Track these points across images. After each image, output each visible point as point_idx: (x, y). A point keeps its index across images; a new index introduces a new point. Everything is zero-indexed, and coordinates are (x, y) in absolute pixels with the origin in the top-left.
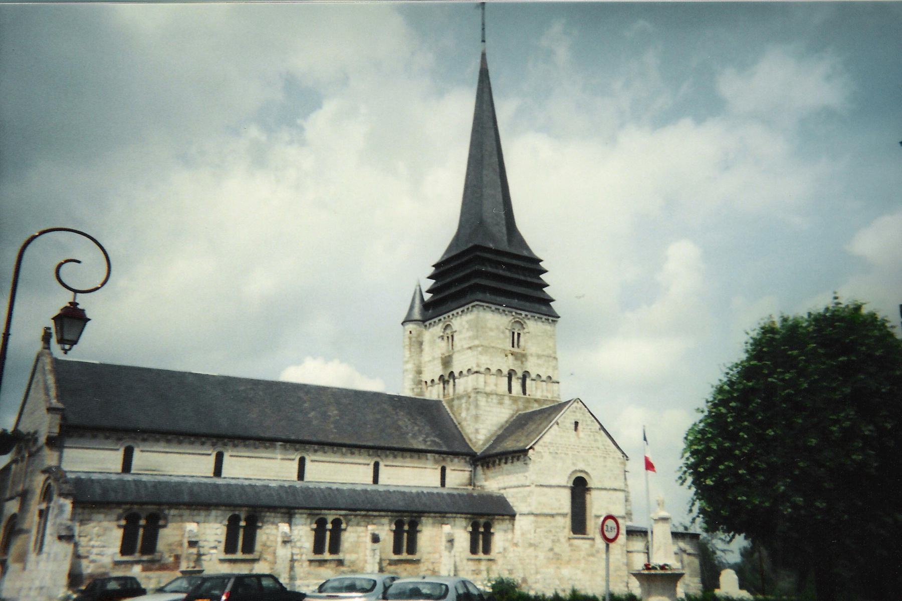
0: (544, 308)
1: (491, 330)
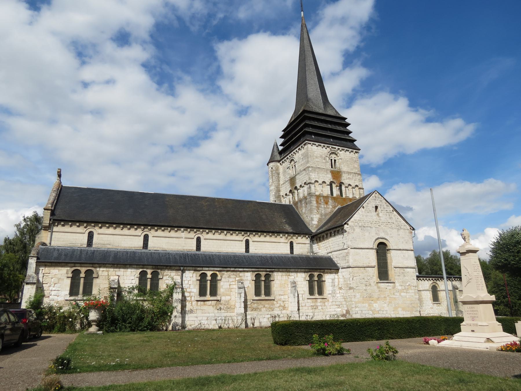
0: (349, 144)
1: (317, 157)
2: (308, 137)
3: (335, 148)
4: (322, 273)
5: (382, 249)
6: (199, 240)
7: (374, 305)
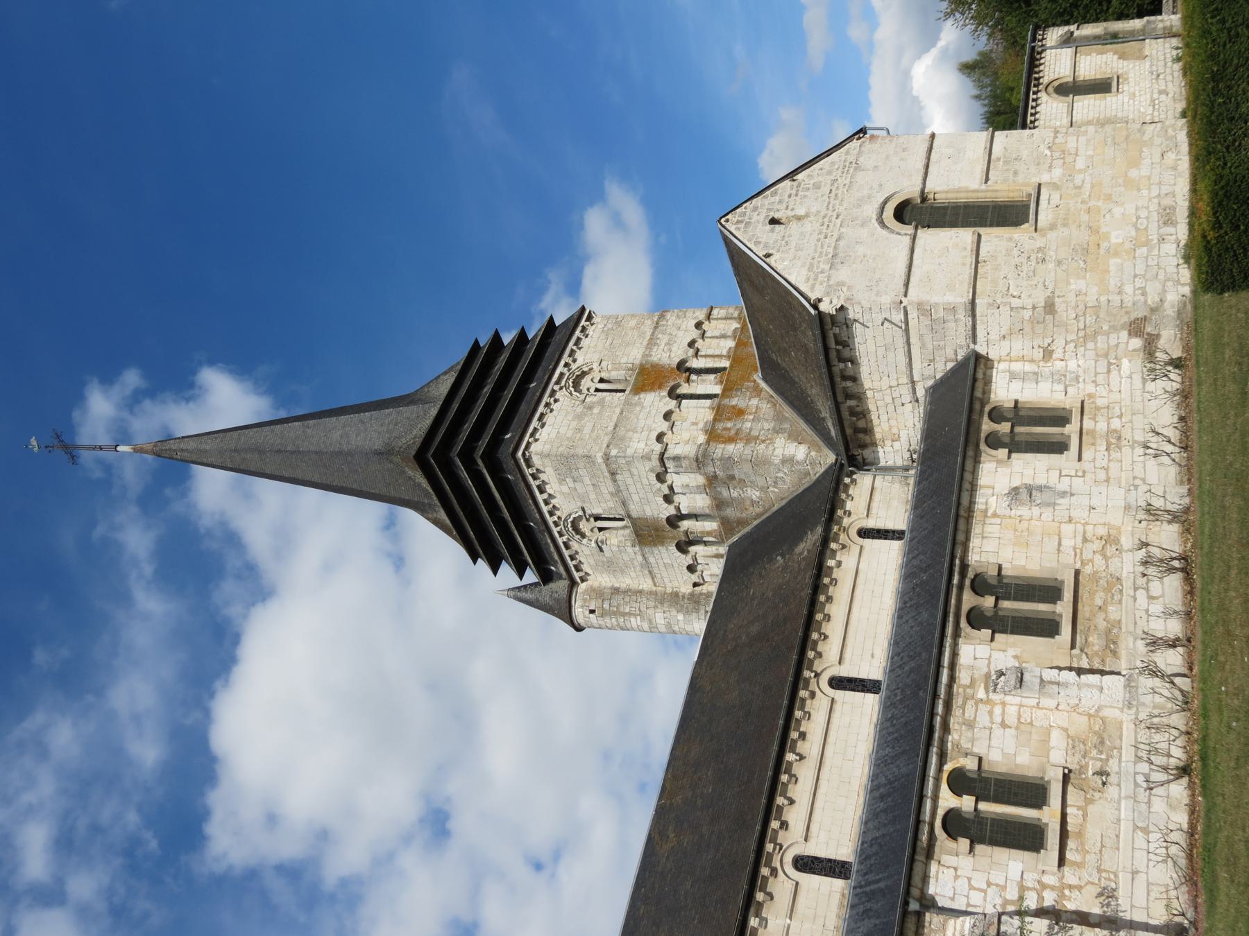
0: (557, 337)
1: (579, 430)
2: (504, 453)
3: (562, 375)
4: (987, 409)
5: (914, 213)
6: (806, 864)
7: (1113, 240)
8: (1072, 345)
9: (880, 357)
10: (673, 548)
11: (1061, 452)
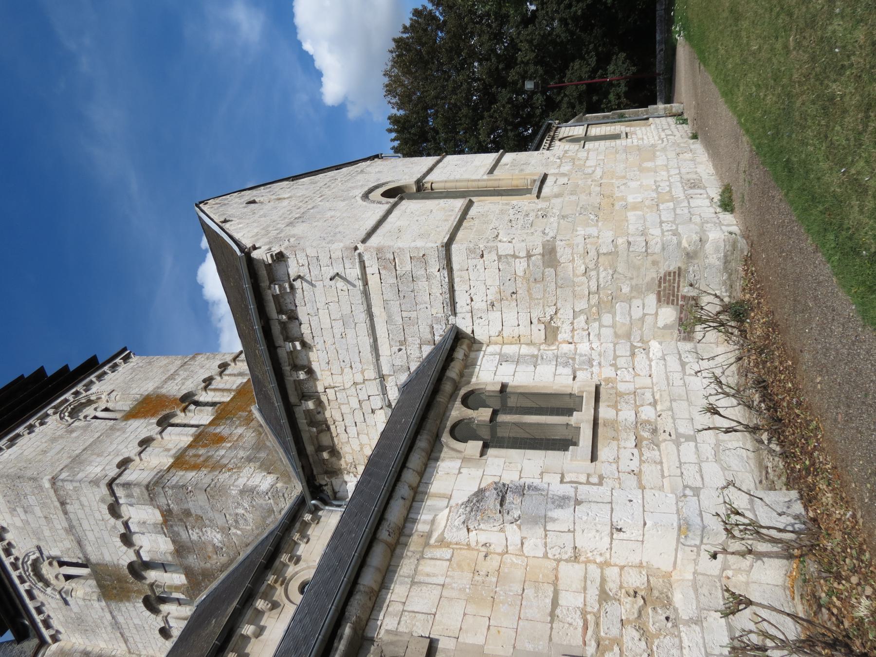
4: (463, 392)
8: (583, 318)
9: (338, 336)
10: (140, 605)
11: (566, 449)
